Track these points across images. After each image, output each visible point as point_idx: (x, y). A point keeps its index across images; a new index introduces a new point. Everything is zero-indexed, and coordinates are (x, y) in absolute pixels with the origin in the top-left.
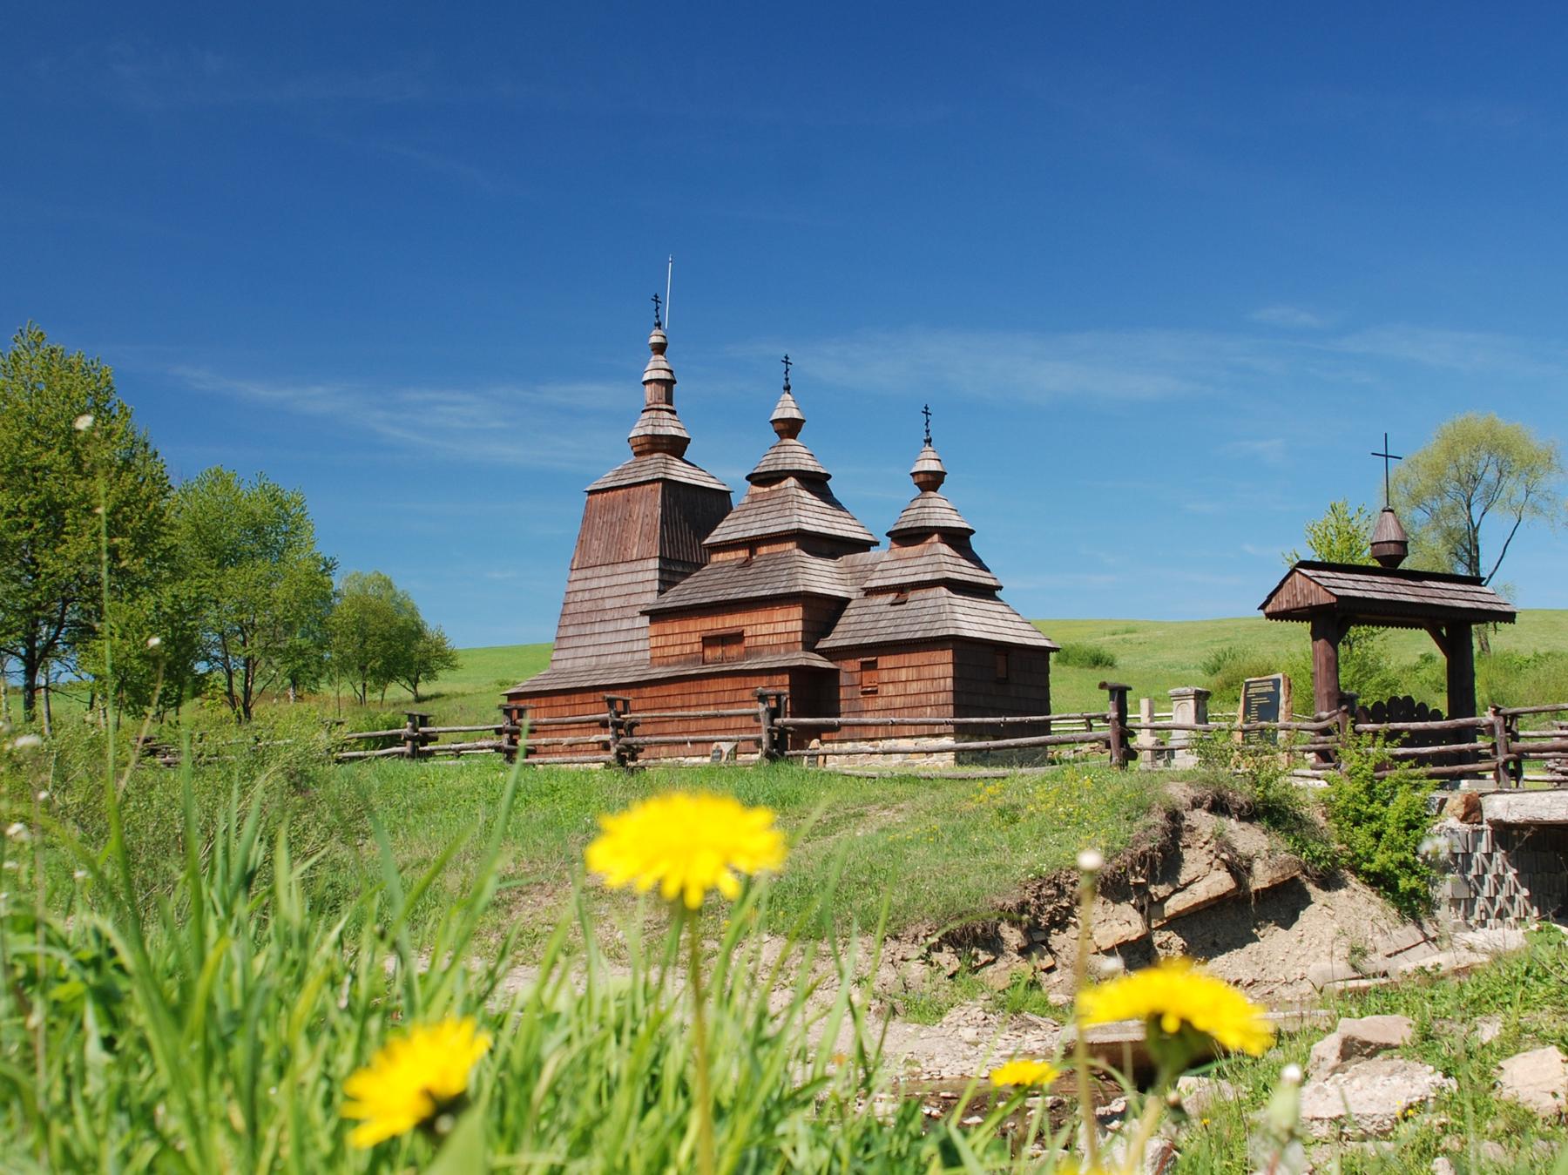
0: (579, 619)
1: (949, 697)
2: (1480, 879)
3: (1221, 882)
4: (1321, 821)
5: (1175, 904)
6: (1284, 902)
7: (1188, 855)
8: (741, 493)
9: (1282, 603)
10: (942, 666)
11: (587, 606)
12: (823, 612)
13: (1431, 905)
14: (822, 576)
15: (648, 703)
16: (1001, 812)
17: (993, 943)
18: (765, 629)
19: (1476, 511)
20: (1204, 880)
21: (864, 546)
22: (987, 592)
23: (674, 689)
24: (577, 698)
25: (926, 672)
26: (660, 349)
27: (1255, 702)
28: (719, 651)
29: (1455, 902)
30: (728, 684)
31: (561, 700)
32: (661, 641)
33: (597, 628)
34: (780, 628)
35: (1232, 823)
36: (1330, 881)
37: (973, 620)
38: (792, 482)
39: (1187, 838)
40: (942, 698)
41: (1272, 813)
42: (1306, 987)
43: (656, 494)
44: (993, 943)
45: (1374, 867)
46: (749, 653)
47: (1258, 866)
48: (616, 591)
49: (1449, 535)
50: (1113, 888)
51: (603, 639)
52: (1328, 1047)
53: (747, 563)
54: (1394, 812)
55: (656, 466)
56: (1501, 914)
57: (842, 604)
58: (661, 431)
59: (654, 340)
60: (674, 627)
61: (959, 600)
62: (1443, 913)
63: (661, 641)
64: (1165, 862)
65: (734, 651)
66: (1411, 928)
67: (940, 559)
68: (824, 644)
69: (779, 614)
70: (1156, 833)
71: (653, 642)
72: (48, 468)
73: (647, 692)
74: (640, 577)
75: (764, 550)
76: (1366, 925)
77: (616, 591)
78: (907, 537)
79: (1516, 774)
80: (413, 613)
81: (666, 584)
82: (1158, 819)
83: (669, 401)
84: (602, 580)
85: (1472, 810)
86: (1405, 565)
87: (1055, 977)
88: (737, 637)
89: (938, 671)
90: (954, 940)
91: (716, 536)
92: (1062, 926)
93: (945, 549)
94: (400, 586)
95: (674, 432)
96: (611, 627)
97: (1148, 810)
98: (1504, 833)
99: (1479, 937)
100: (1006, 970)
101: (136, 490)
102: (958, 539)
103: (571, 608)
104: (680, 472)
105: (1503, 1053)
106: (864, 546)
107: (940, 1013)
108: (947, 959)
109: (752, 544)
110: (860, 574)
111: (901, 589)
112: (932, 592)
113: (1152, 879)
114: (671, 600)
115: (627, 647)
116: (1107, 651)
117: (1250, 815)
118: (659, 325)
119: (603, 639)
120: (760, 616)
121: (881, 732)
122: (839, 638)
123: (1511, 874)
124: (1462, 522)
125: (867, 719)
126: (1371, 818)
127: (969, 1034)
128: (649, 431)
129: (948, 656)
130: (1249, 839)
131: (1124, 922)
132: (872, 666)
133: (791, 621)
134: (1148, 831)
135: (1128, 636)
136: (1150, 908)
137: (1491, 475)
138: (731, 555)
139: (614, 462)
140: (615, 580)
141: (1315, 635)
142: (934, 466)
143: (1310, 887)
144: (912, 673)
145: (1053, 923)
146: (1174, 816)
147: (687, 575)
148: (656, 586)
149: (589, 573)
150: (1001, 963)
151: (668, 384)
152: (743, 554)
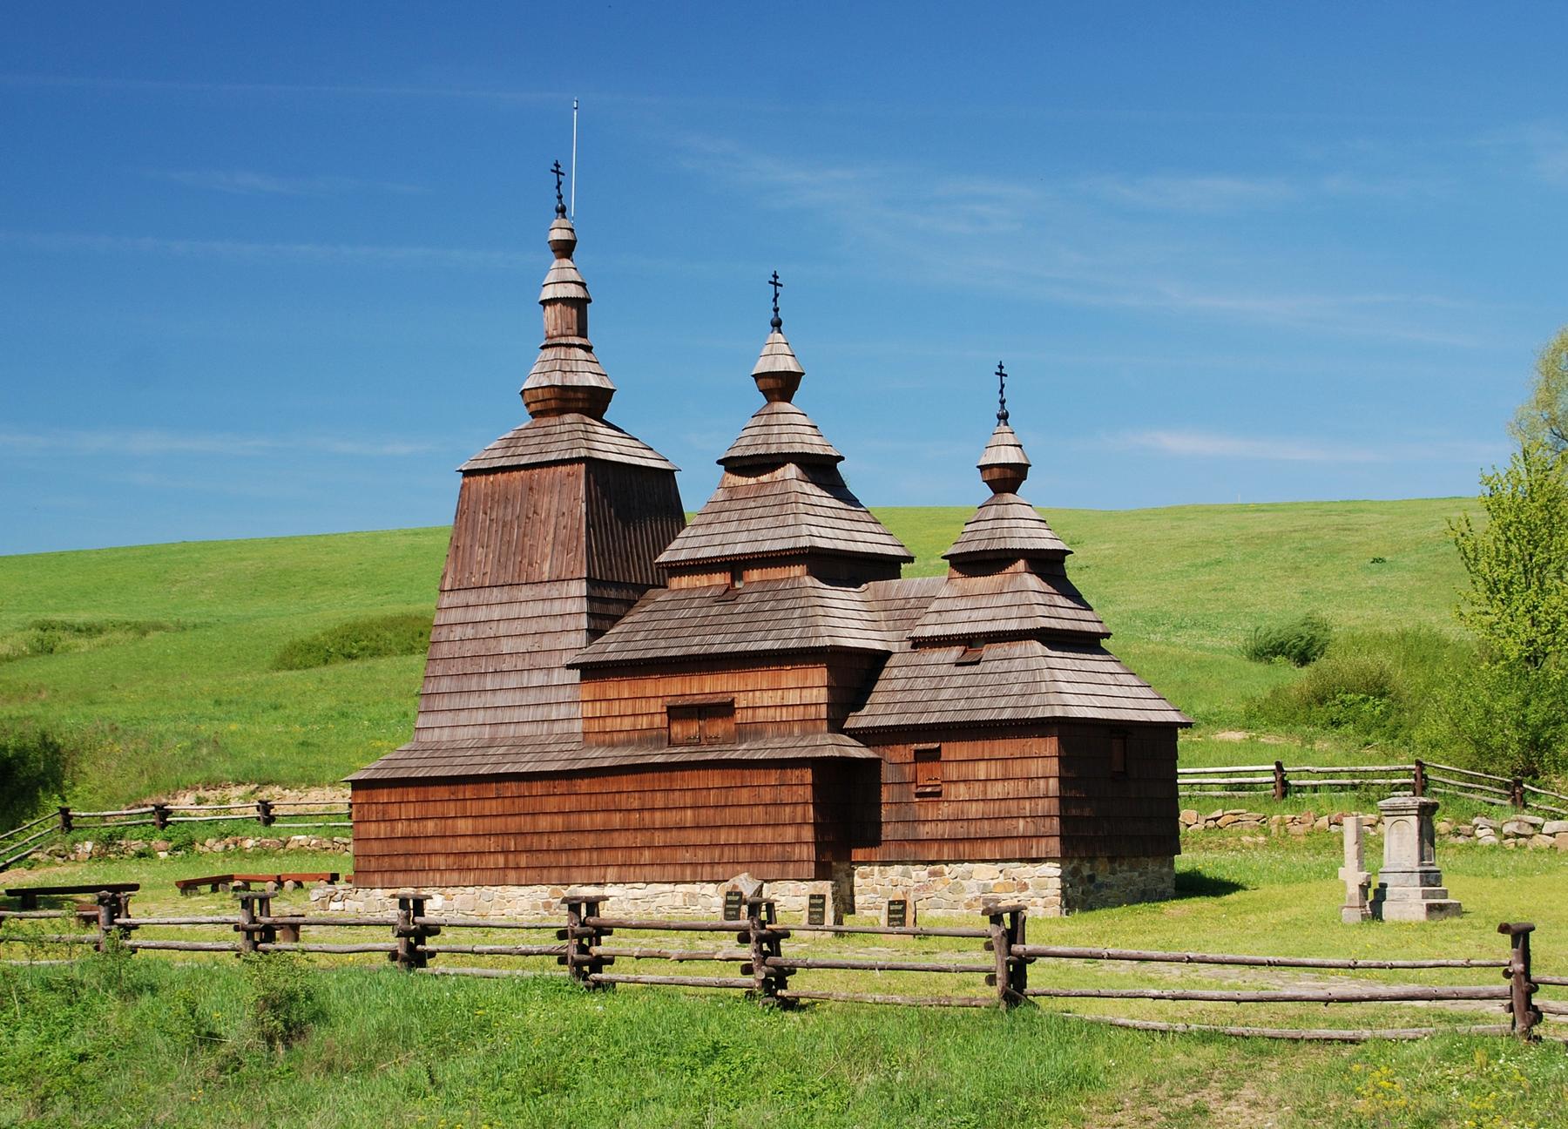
0: (458, 667)
1: (1053, 806)
8: (699, 488)
10: (1042, 763)
11: (470, 649)
12: (855, 673)
14: (848, 617)
15: (585, 802)
18: (767, 698)
21: (886, 567)
22: (1086, 643)
23: (627, 782)
24: (469, 791)
25: (1017, 768)
26: (565, 249)
28: (693, 728)
30: (715, 778)
31: (442, 792)
33: (489, 683)
34: (793, 697)
37: (1084, 691)
38: (791, 471)
40: (1042, 806)
46: (742, 733)
48: (517, 627)
51: (500, 699)
53: (728, 596)
55: (568, 436)
57: (878, 660)
58: (575, 381)
59: (557, 235)
60: (625, 688)
65: (719, 727)
67: (1021, 599)
68: (856, 721)
69: (789, 676)
71: (588, 710)
73: (583, 785)
74: (557, 607)
75: (755, 575)
77: (517, 627)
78: (971, 563)
81: (600, 622)
83: (582, 332)
84: (493, 610)
89: (1036, 767)
91: (678, 550)
93: (1033, 582)
95: (593, 381)
96: (512, 681)
102: (1048, 565)
104: (609, 447)
109: (736, 566)
111: (970, 641)
112: (1019, 648)
114: (612, 647)
118: (562, 211)
119: (500, 699)
120: (761, 678)
121: (947, 851)
122: (876, 713)
125: (925, 831)
128: (557, 379)
129: (1050, 745)
132: (934, 756)
133: (810, 689)
138: (702, 581)
139: (496, 429)
140: (514, 611)
142: (1012, 456)
144: (995, 770)
147: (630, 604)
148: (584, 622)
149: (471, 597)
151: (580, 304)
152: (720, 579)
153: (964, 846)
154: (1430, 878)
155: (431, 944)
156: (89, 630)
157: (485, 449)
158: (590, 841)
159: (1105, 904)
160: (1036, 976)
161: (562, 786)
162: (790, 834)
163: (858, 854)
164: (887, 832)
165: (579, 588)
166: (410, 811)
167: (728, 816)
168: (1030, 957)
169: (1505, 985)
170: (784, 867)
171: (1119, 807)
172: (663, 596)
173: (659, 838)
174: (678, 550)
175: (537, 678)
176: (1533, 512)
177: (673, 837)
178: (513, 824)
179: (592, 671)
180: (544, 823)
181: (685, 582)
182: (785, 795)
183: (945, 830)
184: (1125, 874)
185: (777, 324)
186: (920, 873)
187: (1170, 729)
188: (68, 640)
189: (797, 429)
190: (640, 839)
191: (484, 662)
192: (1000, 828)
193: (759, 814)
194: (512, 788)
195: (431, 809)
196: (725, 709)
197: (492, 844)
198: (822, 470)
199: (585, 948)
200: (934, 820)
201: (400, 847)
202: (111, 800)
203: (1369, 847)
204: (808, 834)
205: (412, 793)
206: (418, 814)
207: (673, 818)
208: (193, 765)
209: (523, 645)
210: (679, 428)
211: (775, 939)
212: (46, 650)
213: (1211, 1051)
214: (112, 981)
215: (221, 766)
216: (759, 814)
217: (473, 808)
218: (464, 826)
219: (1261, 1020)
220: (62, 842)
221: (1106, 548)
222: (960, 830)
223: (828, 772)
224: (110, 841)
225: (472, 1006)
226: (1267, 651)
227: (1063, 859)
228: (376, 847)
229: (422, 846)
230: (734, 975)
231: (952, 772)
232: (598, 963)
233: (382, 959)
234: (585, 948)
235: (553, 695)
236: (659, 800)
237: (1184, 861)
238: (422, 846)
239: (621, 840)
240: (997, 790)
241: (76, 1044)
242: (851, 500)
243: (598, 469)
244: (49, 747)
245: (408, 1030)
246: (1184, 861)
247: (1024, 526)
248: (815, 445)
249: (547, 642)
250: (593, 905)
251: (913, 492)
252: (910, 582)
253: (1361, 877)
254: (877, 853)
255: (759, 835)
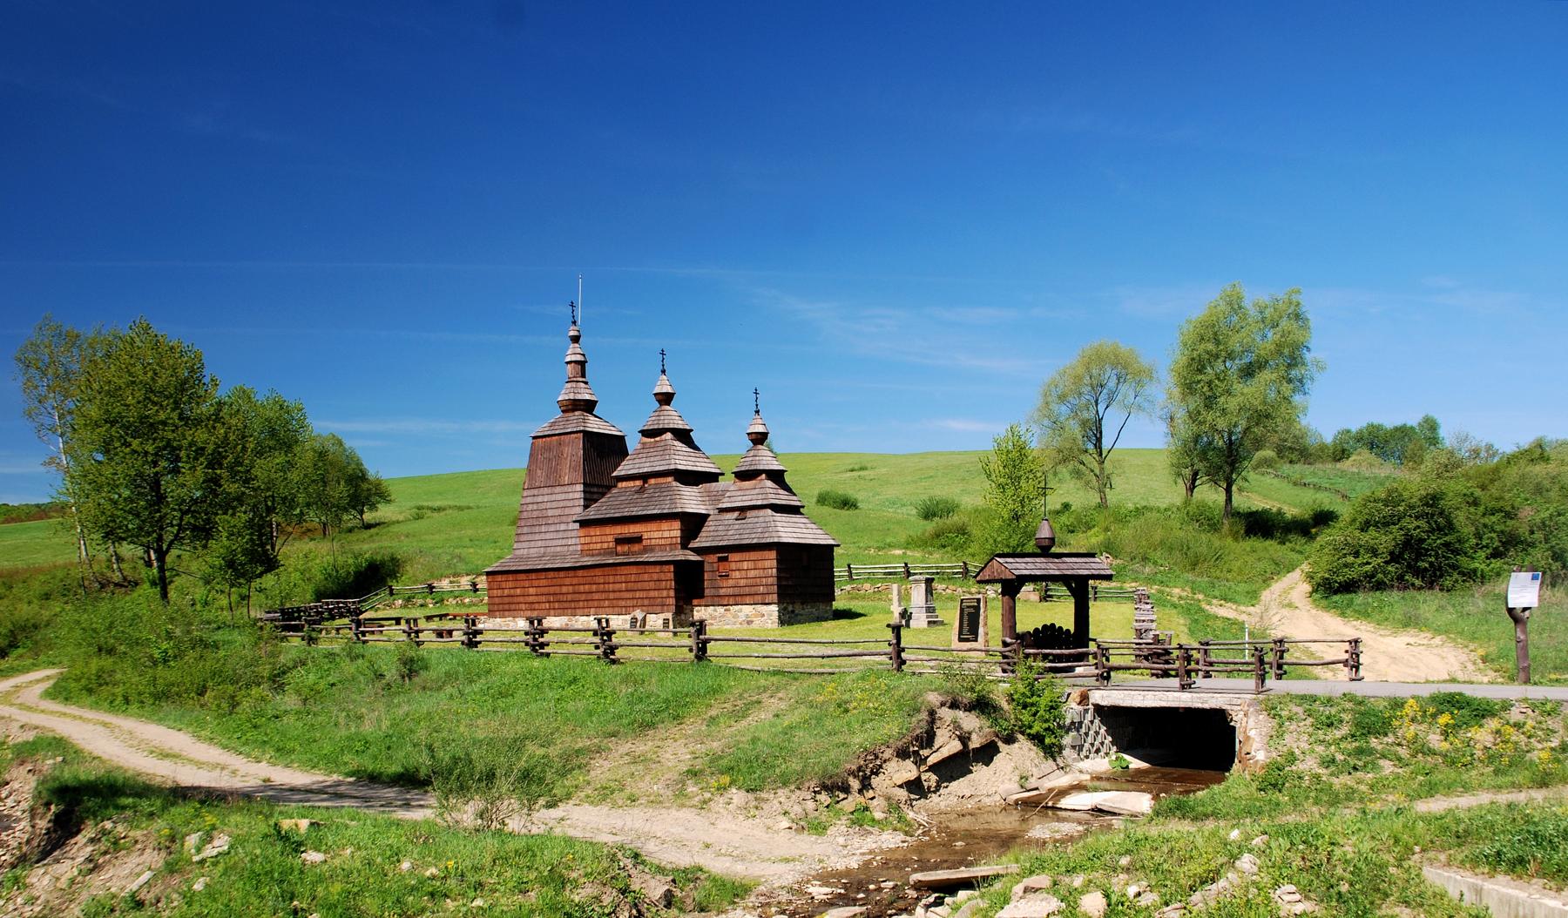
0: (530, 522)
1: (774, 580)
2: (1087, 734)
3: (956, 746)
4: (1005, 706)
5: (932, 760)
6: (987, 753)
7: (938, 732)
8: (633, 443)
9: (986, 575)
10: (770, 561)
11: (535, 514)
12: (692, 524)
13: (1061, 748)
14: (691, 500)
15: (581, 580)
16: (839, 706)
17: (846, 789)
18: (656, 535)
19: (1101, 408)
20: (946, 745)
21: (713, 477)
22: (794, 510)
23: (598, 572)
24: (533, 576)
25: (760, 564)
26: (576, 339)
27: (966, 611)
28: (626, 548)
29: (1073, 747)
30: (634, 570)
31: (523, 576)
32: (588, 540)
33: (543, 529)
34: (666, 534)
35: (960, 714)
36: (1010, 740)
37: (790, 531)
38: (669, 436)
39: (938, 723)
40: (770, 580)
41: (982, 705)
42: (997, 798)
43: (579, 442)
44: (846, 789)
45: (1033, 731)
46: (646, 549)
47: (974, 736)
48: (554, 505)
49: (1084, 423)
50: (903, 754)
51: (548, 536)
52: (1018, 889)
53: (641, 490)
54: (1043, 702)
55: (576, 421)
56: (1098, 751)
57: (702, 518)
58: (579, 397)
59: (572, 333)
60: (597, 531)
61: (779, 517)
62: (1066, 752)
63: (588, 540)
64: (928, 739)
65: (636, 547)
66: (1050, 761)
67: (766, 491)
68: (694, 544)
69: (665, 525)
70: (923, 724)
71: (583, 540)
72: (164, 423)
73: (580, 573)
74: (571, 496)
75: (653, 481)
76: (1028, 763)
77: (554, 505)
78: (744, 476)
79: (1108, 678)
80: (359, 464)
81: (589, 501)
82: (924, 716)
83: (583, 376)
84: (544, 497)
85: (1084, 699)
86: (1054, 550)
87: (875, 802)
88: (638, 540)
89: (767, 564)
90: (825, 787)
91: (621, 470)
92: (877, 774)
93: (769, 483)
94: (348, 444)
95: (587, 397)
96: (552, 528)
97: (919, 711)
98: (1099, 709)
99: (1086, 765)
100: (852, 802)
101: (226, 437)
102: (777, 477)
103: (525, 515)
104: (594, 425)
105: (1082, 893)
106: (713, 477)
107: (825, 828)
108: (824, 798)
109: (645, 477)
110: (715, 497)
111: (742, 509)
112: (762, 512)
113: (922, 747)
114: (593, 513)
115: (563, 542)
116: (852, 493)
117: (970, 708)
118: (574, 323)
119: (548, 536)
120: (653, 526)
121: (732, 601)
122: (702, 541)
123: (1103, 729)
124: (1092, 414)
125: (722, 592)
126: (1032, 705)
127: (841, 840)
128: (571, 397)
129: (773, 554)
130: (970, 721)
131: (906, 771)
132: (725, 559)
133: (673, 531)
134: (920, 720)
135: (862, 473)
136: (920, 761)
137: (1112, 384)
138: (631, 484)
139: (547, 418)
140: (553, 497)
141: (1003, 594)
142: (761, 429)
143: (1000, 744)
144: (751, 565)
145: (872, 773)
146: (932, 713)
147: (603, 494)
148: (582, 502)
149: (536, 492)
150: (850, 798)
151: (582, 364)
152: (639, 483)
153: (738, 598)
154: (930, 610)
155: (479, 638)
156: (439, 509)
157: (542, 427)
158: (583, 597)
159: (800, 622)
160: (712, 648)
161: (571, 573)
162: (665, 593)
163: (695, 602)
164: (707, 592)
165: (580, 487)
166: (510, 584)
167: (639, 585)
168: (708, 641)
169: (890, 649)
170: (653, 606)
171: (806, 582)
172: (614, 491)
173: (612, 596)
174: (621, 470)
175: (563, 527)
176: (1015, 454)
177: (617, 595)
178: (552, 590)
179: (584, 524)
180: (564, 589)
181: (624, 484)
182: (663, 576)
183: (730, 591)
184: (808, 609)
185: (663, 372)
186: (721, 610)
187: (830, 548)
188: (429, 513)
189: (673, 417)
190: (604, 596)
191: (541, 519)
192: (753, 590)
193: (652, 585)
194: (551, 574)
195: (518, 584)
196: (639, 540)
197: (544, 599)
198: (684, 436)
199: (536, 641)
200: (726, 587)
201: (506, 600)
202: (415, 583)
203: (904, 597)
204: (672, 593)
205: (511, 577)
206: (512, 584)
207: (617, 586)
208: (449, 567)
209: (557, 512)
210: (619, 417)
211: (610, 634)
212: (419, 517)
213: (775, 679)
214: (349, 655)
215: (461, 567)
216: (652, 585)
217: (536, 583)
218: (532, 591)
219: (788, 665)
220: (389, 600)
221: (884, 470)
222: (737, 591)
223: (679, 566)
224: (409, 600)
225: (487, 662)
226: (928, 514)
227: (778, 604)
228: (497, 600)
229: (516, 600)
230: (592, 649)
231: (733, 566)
232: (542, 645)
233: (458, 645)
234: (536, 641)
235: (569, 534)
236: (611, 579)
237: (838, 604)
238: (516, 600)
239: (596, 596)
240: (752, 574)
241: (331, 679)
242: (696, 448)
243: (589, 437)
244: (393, 559)
245: (457, 673)
246: (838, 604)
247: (767, 461)
248: (680, 425)
249: (567, 511)
250: (540, 622)
251: (721, 446)
252: (722, 483)
253: (900, 609)
254: (703, 601)
255: (652, 594)
